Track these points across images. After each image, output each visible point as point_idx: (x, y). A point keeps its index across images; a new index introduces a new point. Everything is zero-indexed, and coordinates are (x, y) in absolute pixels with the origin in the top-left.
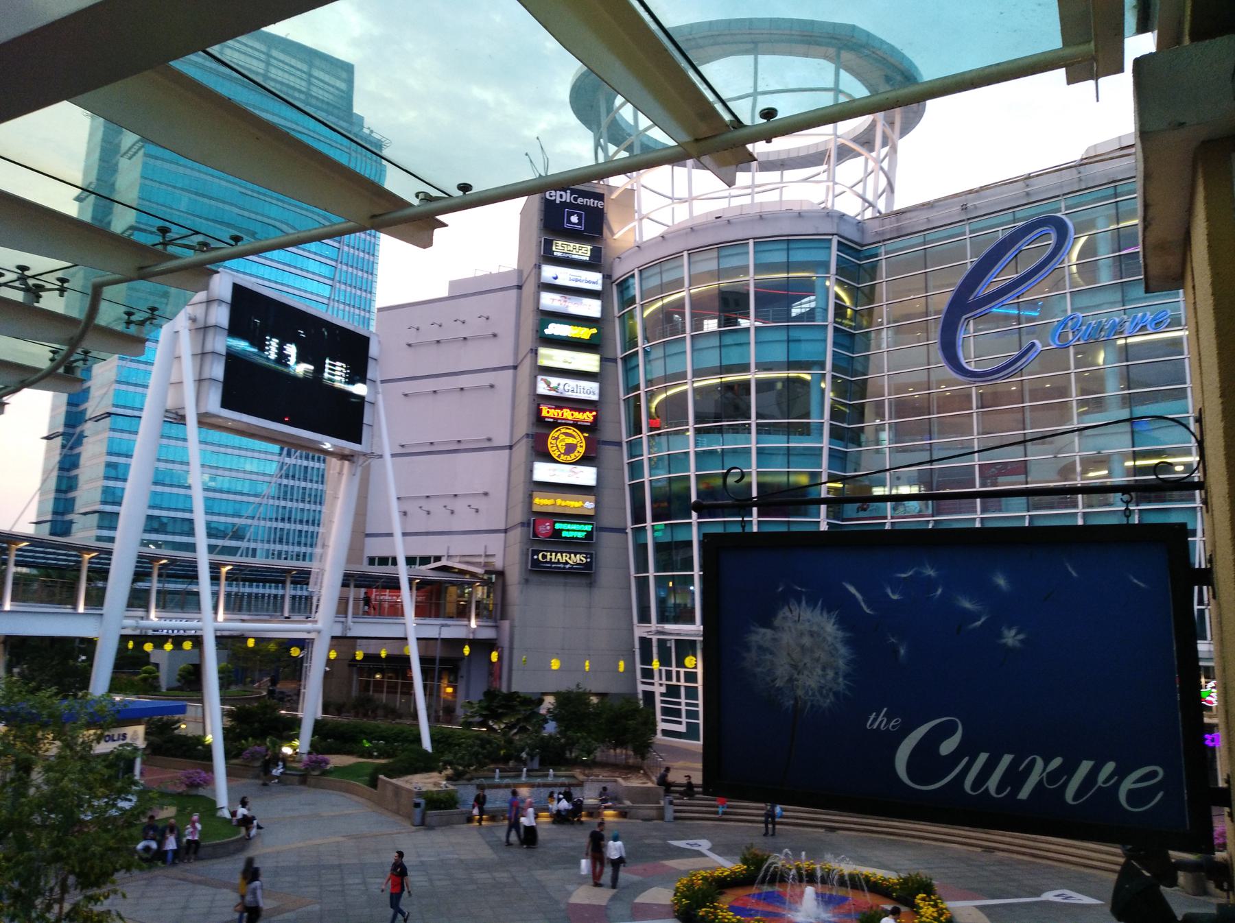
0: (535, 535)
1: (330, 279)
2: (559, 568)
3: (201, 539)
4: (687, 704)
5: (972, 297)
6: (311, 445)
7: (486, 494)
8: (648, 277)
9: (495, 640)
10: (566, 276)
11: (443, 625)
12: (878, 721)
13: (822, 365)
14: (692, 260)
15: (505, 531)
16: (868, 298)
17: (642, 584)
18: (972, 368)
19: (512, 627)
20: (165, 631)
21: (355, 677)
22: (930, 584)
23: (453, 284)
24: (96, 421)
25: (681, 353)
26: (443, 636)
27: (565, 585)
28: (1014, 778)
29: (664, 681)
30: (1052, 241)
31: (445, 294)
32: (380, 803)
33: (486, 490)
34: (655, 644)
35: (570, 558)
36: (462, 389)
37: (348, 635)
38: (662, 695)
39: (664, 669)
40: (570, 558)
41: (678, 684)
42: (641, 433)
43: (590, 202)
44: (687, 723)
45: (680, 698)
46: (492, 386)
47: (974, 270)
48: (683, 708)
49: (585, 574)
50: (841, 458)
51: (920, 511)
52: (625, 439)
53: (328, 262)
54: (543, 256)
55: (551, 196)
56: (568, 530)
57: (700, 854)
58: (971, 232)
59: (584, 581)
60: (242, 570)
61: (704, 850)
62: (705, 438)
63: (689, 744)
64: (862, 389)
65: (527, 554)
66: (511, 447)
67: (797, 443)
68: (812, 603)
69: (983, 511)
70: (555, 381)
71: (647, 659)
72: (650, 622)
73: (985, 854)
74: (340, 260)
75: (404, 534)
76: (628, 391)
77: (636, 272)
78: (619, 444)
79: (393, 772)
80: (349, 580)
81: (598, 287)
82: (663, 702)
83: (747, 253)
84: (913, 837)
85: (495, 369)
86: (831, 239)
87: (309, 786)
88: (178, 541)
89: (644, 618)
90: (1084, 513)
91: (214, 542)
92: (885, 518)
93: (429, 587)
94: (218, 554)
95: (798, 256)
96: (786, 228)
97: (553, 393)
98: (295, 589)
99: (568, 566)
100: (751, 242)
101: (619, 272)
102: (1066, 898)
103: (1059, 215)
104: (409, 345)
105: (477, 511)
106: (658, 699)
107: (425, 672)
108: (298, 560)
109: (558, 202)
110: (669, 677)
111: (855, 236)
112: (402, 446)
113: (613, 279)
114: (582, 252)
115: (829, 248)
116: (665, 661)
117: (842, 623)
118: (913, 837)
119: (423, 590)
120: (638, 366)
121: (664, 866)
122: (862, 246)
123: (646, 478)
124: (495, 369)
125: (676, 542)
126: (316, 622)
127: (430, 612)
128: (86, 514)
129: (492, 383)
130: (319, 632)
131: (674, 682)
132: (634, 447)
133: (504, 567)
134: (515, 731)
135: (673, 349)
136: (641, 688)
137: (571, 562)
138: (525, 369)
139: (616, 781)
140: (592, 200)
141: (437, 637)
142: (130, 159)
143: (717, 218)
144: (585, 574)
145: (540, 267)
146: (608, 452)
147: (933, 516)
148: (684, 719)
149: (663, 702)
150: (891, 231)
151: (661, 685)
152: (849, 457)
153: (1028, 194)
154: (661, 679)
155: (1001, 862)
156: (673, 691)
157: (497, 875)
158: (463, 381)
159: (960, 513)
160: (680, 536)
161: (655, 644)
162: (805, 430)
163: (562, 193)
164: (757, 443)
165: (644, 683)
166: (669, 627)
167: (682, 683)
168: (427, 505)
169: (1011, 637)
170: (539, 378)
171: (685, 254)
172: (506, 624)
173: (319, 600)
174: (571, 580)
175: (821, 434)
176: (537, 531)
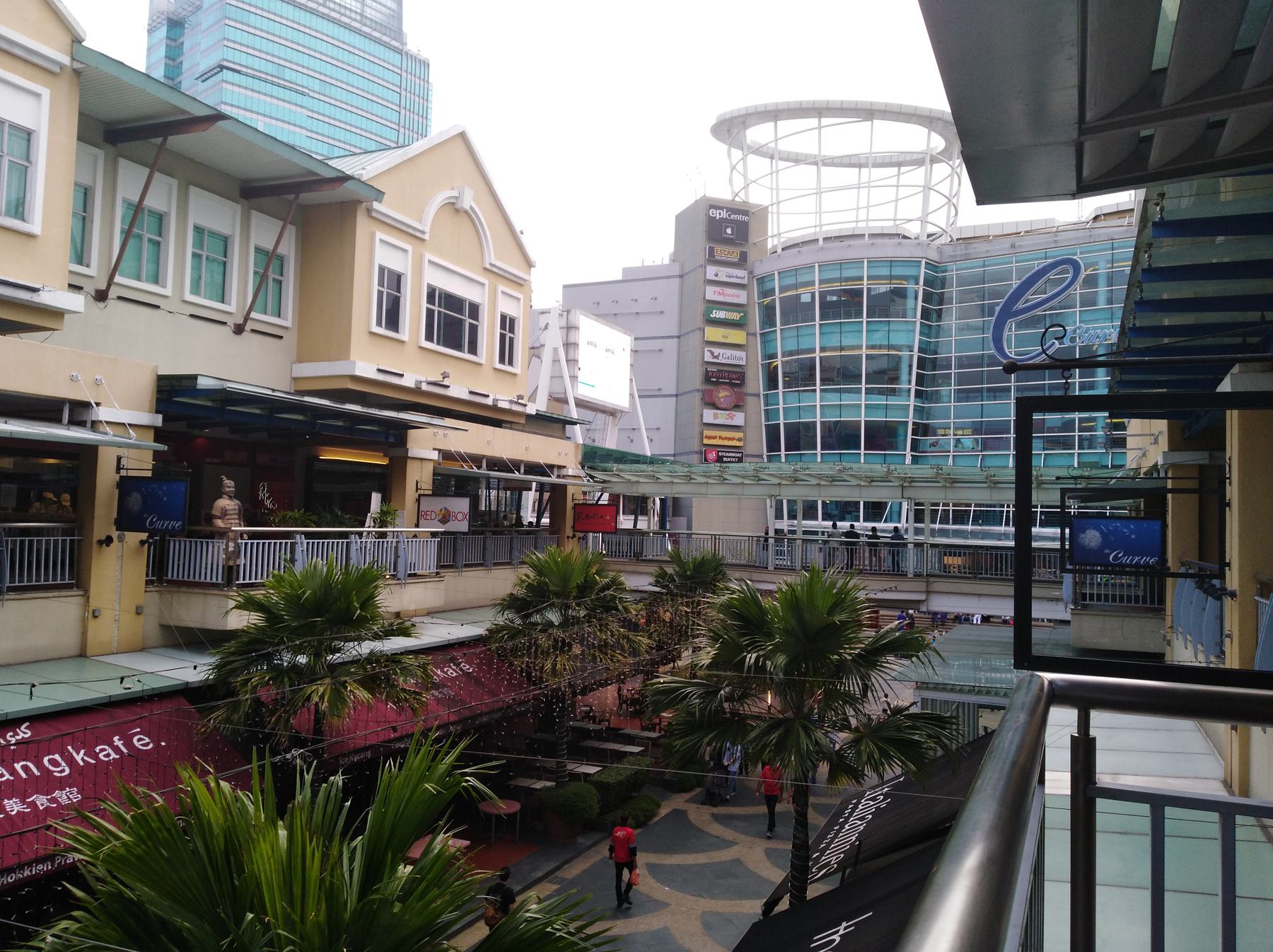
7: (658, 429)
10: (724, 274)
12: (1107, 551)
13: (911, 349)
22: (1118, 527)
23: (625, 271)
28: (1132, 560)
30: (1070, 275)
31: (620, 277)
43: (740, 217)
56: (727, 457)
58: (1017, 262)
62: (828, 395)
67: (893, 401)
68: (1094, 529)
70: (717, 351)
78: (758, 395)
85: (662, 338)
92: (950, 452)
95: (898, 271)
97: (715, 360)
101: (760, 270)
103: (1075, 257)
114: (733, 254)
117: (1100, 533)
124: (662, 338)
145: (705, 267)
146: (750, 401)
150: (961, 255)
152: (925, 410)
159: (999, 450)
169: (1133, 537)
170: (706, 349)
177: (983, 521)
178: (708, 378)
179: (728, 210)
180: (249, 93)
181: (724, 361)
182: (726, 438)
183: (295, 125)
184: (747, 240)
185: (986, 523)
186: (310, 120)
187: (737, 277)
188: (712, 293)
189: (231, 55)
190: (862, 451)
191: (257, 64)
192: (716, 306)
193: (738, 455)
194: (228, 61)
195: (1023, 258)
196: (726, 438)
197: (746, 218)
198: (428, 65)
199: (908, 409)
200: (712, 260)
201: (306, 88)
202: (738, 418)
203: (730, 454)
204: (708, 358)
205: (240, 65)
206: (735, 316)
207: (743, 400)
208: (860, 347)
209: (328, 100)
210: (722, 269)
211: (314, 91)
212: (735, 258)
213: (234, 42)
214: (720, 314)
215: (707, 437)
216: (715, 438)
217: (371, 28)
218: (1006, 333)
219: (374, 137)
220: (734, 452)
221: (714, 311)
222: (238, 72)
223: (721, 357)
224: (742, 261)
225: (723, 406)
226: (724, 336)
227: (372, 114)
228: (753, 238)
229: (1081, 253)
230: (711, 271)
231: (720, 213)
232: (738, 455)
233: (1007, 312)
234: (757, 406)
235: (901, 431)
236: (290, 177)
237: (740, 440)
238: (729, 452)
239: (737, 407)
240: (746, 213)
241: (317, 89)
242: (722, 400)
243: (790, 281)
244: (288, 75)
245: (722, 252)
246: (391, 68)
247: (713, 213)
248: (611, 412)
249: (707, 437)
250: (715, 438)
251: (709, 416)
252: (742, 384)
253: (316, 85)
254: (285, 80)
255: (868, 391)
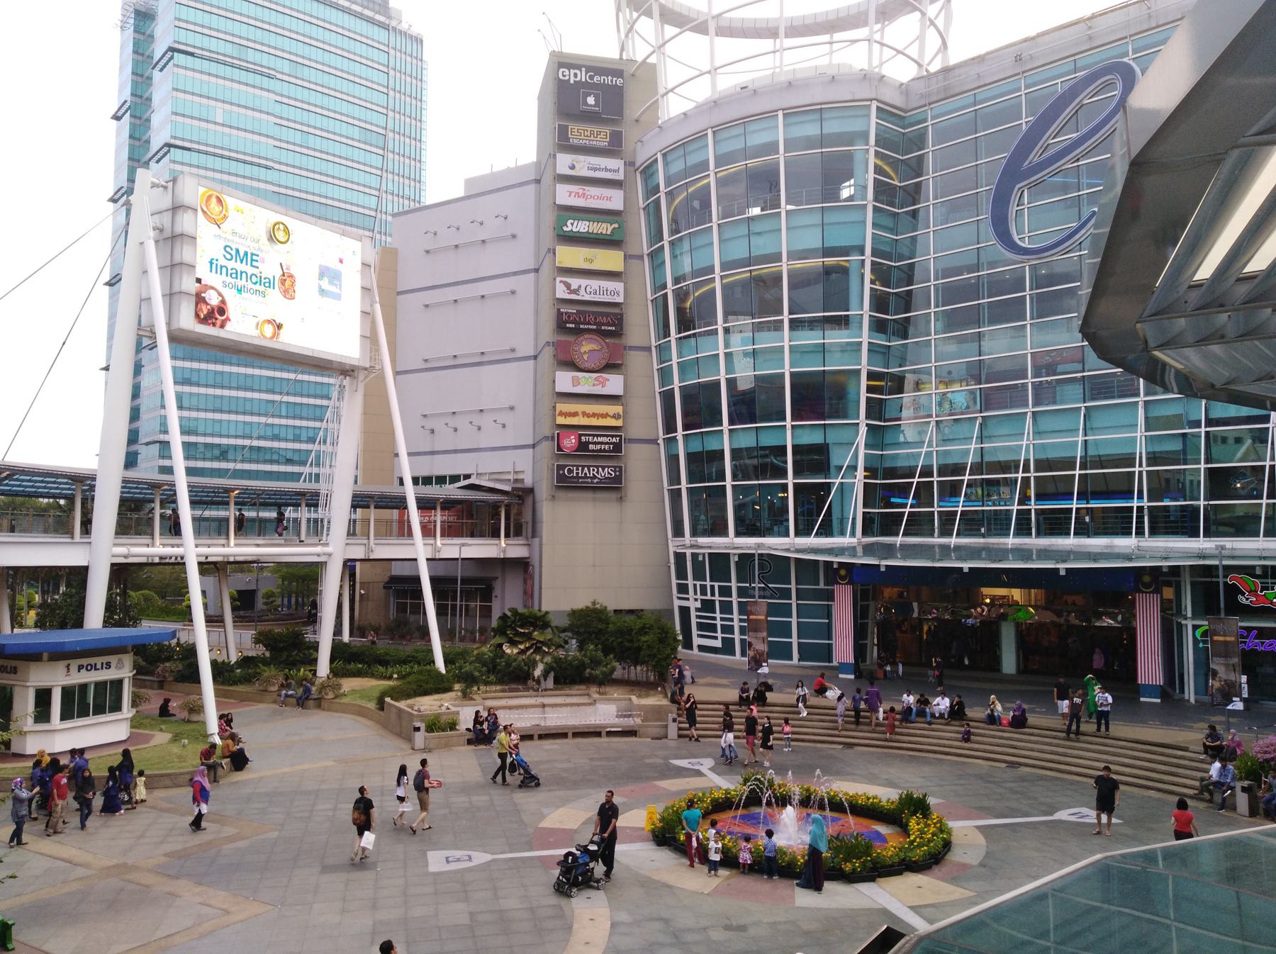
0: (559, 449)
1: (376, 189)
2: (587, 483)
3: (179, 462)
4: (722, 619)
5: (1027, 163)
6: (329, 366)
7: (512, 408)
8: (673, 161)
9: (529, 558)
10: (584, 165)
11: (463, 545)
13: (861, 250)
14: (717, 139)
15: (534, 446)
16: (915, 171)
17: (675, 495)
18: (1025, 244)
19: (541, 545)
20: (173, 558)
21: (392, 599)
23: (469, 183)
24: (151, 349)
25: (707, 245)
26: (463, 556)
27: (594, 500)
29: (699, 596)
31: (460, 193)
32: (385, 725)
33: (512, 404)
34: (689, 558)
35: (598, 472)
36: (483, 296)
37: (437, 557)
38: (697, 610)
39: (698, 583)
40: (598, 472)
41: (713, 598)
42: (669, 336)
43: (608, 80)
44: (722, 638)
45: (715, 612)
46: (513, 292)
47: (1029, 130)
48: (719, 623)
49: (614, 486)
50: (884, 353)
51: (967, 407)
52: (654, 343)
53: (373, 171)
54: (558, 144)
55: (564, 76)
56: (595, 443)
57: (699, 773)
58: (1026, 87)
59: (614, 495)
60: (259, 495)
61: (704, 769)
63: (707, 657)
64: (908, 275)
65: (553, 470)
66: (535, 357)
69: (1036, 404)
70: (575, 282)
71: (681, 574)
72: (683, 536)
73: (1009, 770)
74: (385, 168)
75: (410, 454)
76: (655, 290)
77: (659, 156)
78: (648, 349)
79: (399, 694)
80: (359, 501)
81: (620, 176)
82: (698, 617)
83: (777, 127)
84: (935, 752)
85: (515, 274)
86: (870, 105)
87: (324, 710)
88: (277, 470)
89: (678, 532)
90: (1146, 402)
91: (193, 464)
92: (931, 416)
93: (459, 507)
94: (229, 478)
95: (832, 127)
96: (817, 95)
98: (309, 511)
99: (596, 481)
100: (780, 114)
102: (1082, 817)
103: (1125, 60)
104: (428, 252)
105: (504, 426)
106: (693, 614)
107: (437, 594)
108: (310, 481)
109: (572, 82)
110: (704, 592)
111: (898, 100)
112: (426, 361)
113: (638, 164)
114: (601, 136)
115: (868, 116)
116: (699, 575)
118: (935, 752)
119: (453, 509)
120: (664, 262)
121: (655, 786)
122: (906, 112)
123: (676, 384)
124: (515, 274)
125: (708, 452)
126: (327, 545)
127: (463, 532)
128: (147, 444)
129: (514, 288)
130: (330, 555)
131: (709, 597)
132: (663, 350)
133: (533, 484)
134: (532, 650)
135: (699, 241)
136: (677, 603)
137: (599, 476)
138: (546, 270)
139: (630, 699)
140: (610, 78)
141: (457, 557)
142: (161, 70)
143: (742, 88)
144: (614, 486)
145: (555, 156)
147: (981, 412)
148: (719, 635)
149: (698, 617)
151: (696, 600)
152: (892, 352)
153: (1090, 38)
154: (696, 593)
155: (1023, 779)
156: (708, 606)
157: (475, 798)
158: (484, 288)
160: (712, 445)
161: (689, 558)
162: (843, 322)
163: (576, 71)
164: (790, 341)
165: (679, 598)
166: (703, 540)
167: (717, 598)
168: (453, 422)
170: (558, 279)
171: (710, 132)
172: (536, 540)
173: (329, 522)
174: (599, 495)
175: (861, 327)
176: (562, 445)
177: (989, 530)
178: (562, 324)
179: (589, 69)
180: (205, 78)
181: (587, 298)
182: (594, 415)
183: (261, 111)
184: (620, 113)
185: (216, 490)
186: (278, 105)
187: (606, 170)
188: (566, 195)
189: (183, 36)
190: (788, 422)
191: (214, 45)
192: (572, 214)
193: (614, 440)
194: (179, 43)
195: (1036, 78)
196: (594, 415)
197: (619, 81)
198: (422, 41)
199: (860, 350)
200: (565, 144)
201: (274, 70)
202: (614, 384)
203: (600, 439)
204: (561, 293)
205: (194, 47)
206: (605, 228)
207: (622, 357)
208: (777, 257)
209: (299, 82)
210: (581, 158)
211: (283, 73)
212: (602, 141)
213: (187, 22)
214: (582, 227)
215: (561, 414)
216: (575, 414)
217: (362, 6)
218: (1013, 208)
219: (356, 122)
220: (607, 436)
221: (570, 222)
222: (192, 54)
223: (582, 291)
224: (614, 148)
225: (587, 365)
226: (586, 260)
227: (354, 97)
228: (633, 109)
229: (1135, 52)
230: (564, 163)
231: (575, 75)
232: (614, 440)
233: (1013, 174)
234: (642, 367)
235: (851, 388)
236: (1114, 455)
237: (616, 417)
238: (597, 436)
239: (611, 367)
240: (618, 73)
241: (286, 70)
242: (585, 357)
243: (677, 167)
244: (251, 55)
245: (580, 133)
246: (376, 45)
247: (564, 74)
248: (346, 371)
249: (561, 414)
250: (575, 414)
251: (565, 381)
252: (618, 334)
253: (286, 67)
254: (247, 62)
255: (795, 324)
